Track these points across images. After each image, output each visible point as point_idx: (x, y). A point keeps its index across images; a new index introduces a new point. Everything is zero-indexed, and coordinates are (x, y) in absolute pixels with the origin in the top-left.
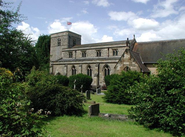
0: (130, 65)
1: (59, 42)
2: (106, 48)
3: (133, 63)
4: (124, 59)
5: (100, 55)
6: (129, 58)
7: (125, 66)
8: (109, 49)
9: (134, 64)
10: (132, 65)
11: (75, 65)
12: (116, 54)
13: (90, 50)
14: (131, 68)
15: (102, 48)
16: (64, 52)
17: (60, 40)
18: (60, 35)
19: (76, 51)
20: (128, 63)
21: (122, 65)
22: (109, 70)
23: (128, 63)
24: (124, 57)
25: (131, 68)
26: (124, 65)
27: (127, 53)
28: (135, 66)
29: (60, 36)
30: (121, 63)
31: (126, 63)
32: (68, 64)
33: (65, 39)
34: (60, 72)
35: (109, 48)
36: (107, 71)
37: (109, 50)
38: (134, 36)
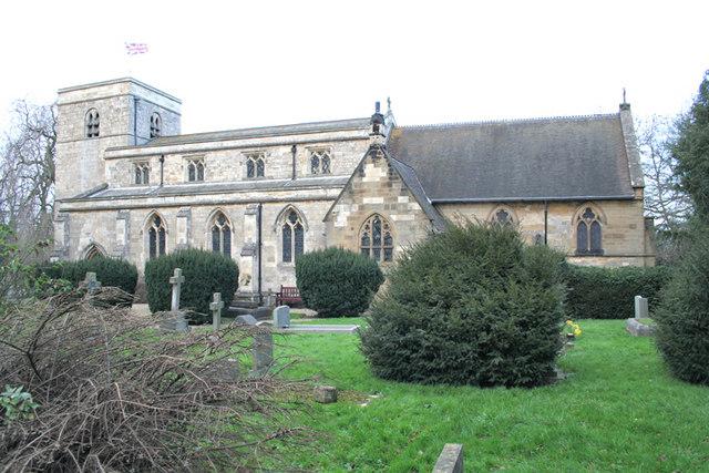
1: (94, 122)
3: (401, 199)
9: (405, 205)
10: (394, 207)
14: (394, 217)
15: (268, 146)
18: (103, 91)
20: (380, 200)
21: (355, 208)
23: (380, 200)
24: (362, 176)
25: (394, 217)
26: (362, 208)
28: (407, 212)
29: (95, 97)
33: (118, 110)
34: (97, 241)
35: (294, 145)
37: (294, 151)
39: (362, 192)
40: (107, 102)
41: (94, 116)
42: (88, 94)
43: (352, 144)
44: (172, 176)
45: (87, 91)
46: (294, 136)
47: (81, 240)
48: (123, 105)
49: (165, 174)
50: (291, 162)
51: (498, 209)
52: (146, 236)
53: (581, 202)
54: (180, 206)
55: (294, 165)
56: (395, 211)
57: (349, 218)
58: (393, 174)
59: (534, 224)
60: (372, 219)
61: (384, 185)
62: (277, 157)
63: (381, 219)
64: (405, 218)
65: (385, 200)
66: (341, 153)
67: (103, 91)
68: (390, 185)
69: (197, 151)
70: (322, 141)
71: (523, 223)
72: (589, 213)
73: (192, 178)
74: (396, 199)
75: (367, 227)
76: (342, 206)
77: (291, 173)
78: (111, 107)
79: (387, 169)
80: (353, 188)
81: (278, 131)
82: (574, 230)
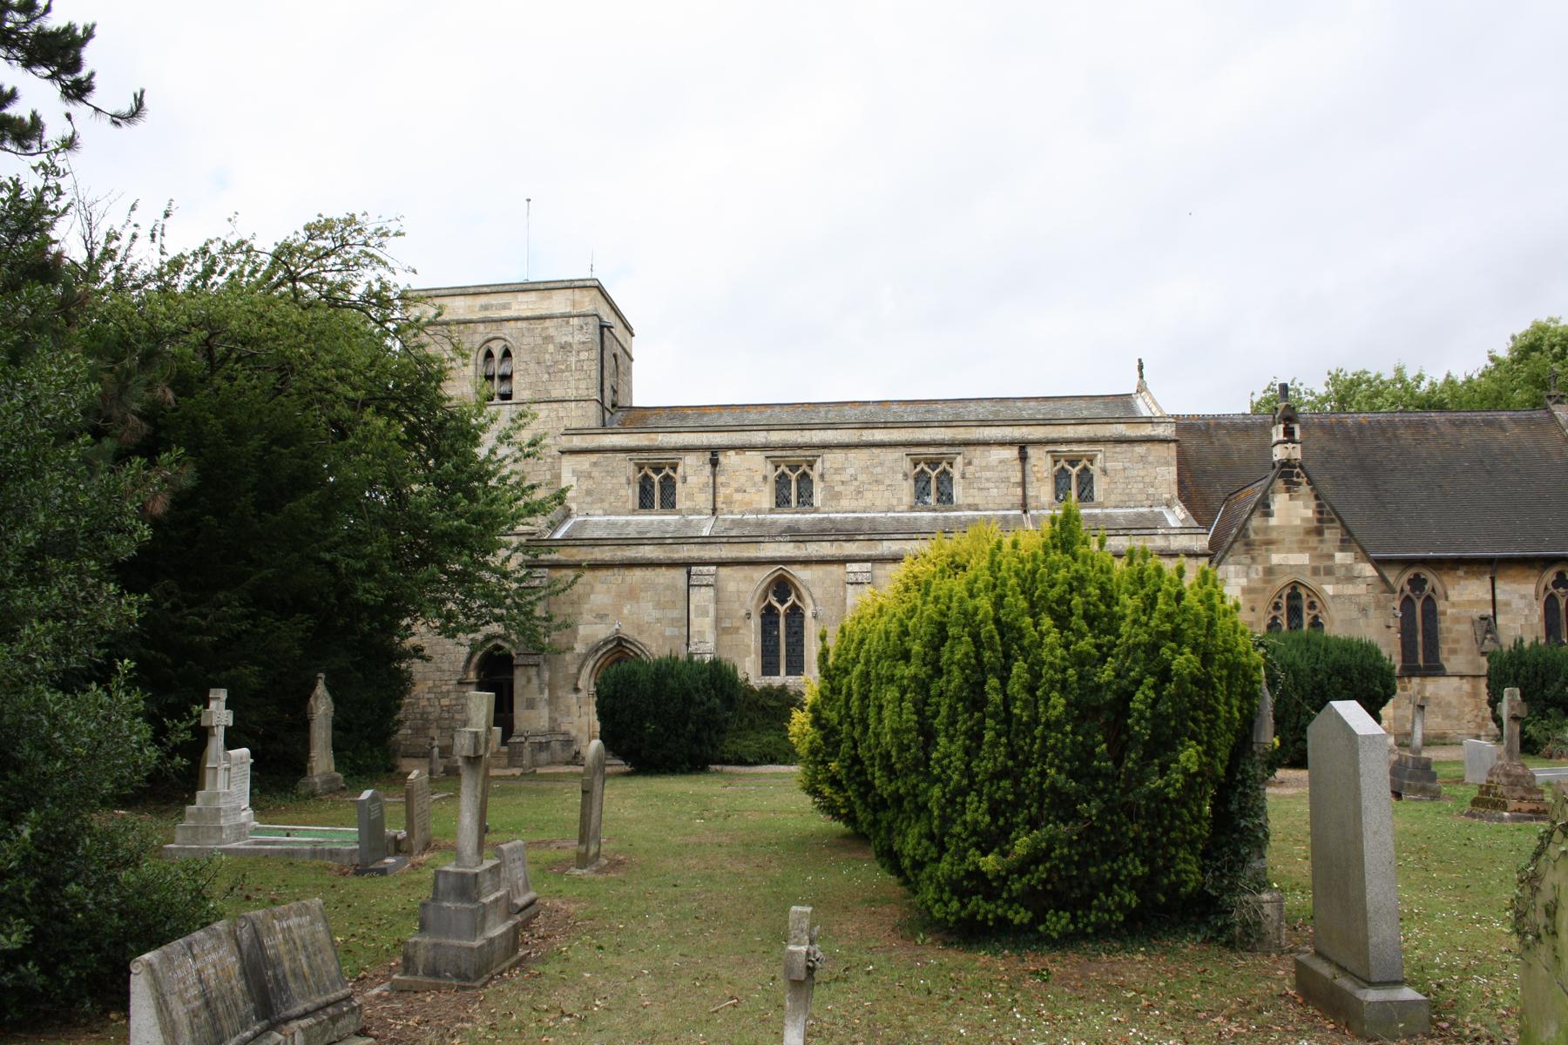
0: (1315, 571)
1: (498, 368)
2: (1002, 444)
3: (1341, 558)
4: (1267, 529)
5: (805, 499)
6: (1305, 520)
7: (1282, 581)
8: (1031, 451)
9: (1348, 568)
10: (1329, 571)
11: (800, 574)
12: (799, 495)
13: (859, 457)
14: (1329, 589)
15: (967, 444)
16: (584, 462)
17: (507, 354)
18: (523, 305)
19: (714, 455)
20: (1303, 559)
21: (1257, 572)
22: (796, 613)
23: (1303, 559)
24: (1268, 514)
25: (1329, 589)
26: (1270, 571)
27: (1288, 490)
28: (1351, 578)
29: (505, 314)
30: (1253, 559)
31: (1292, 559)
32: (721, 564)
33: (565, 347)
34: (628, 632)
35: (1023, 446)
36: (782, 621)
37: (1023, 458)
38: (1141, 367)
39: (1269, 543)
40: (538, 325)
41: (497, 353)
42: (485, 308)
43: (1140, 449)
44: (738, 497)
45: (483, 300)
46: (867, 423)
47: (583, 630)
48: (579, 337)
49: (722, 492)
50: (1017, 477)
51: (1409, 574)
52: (755, 623)
53: (1548, 562)
54: (844, 561)
55: (1023, 484)
56: (1332, 578)
57: (1247, 591)
58: (1326, 514)
59: (1472, 598)
60: (1288, 591)
61: (1308, 532)
62: (987, 468)
63: (1303, 591)
64: (1349, 589)
65: (1312, 557)
66: (1119, 466)
67: (523, 305)
68: (1319, 532)
69: (799, 447)
70: (1080, 441)
71: (1454, 595)
72: (1417, 583)
73: (782, 501)
74: (1331, 557)
75: (1277, 607)
76: (1232, 568)
77: (1018, 500)
78: (548, 339)
79: (1313, 504)
80: (1252, 536)
81: (1001, 410)
82: (1539, 610)
